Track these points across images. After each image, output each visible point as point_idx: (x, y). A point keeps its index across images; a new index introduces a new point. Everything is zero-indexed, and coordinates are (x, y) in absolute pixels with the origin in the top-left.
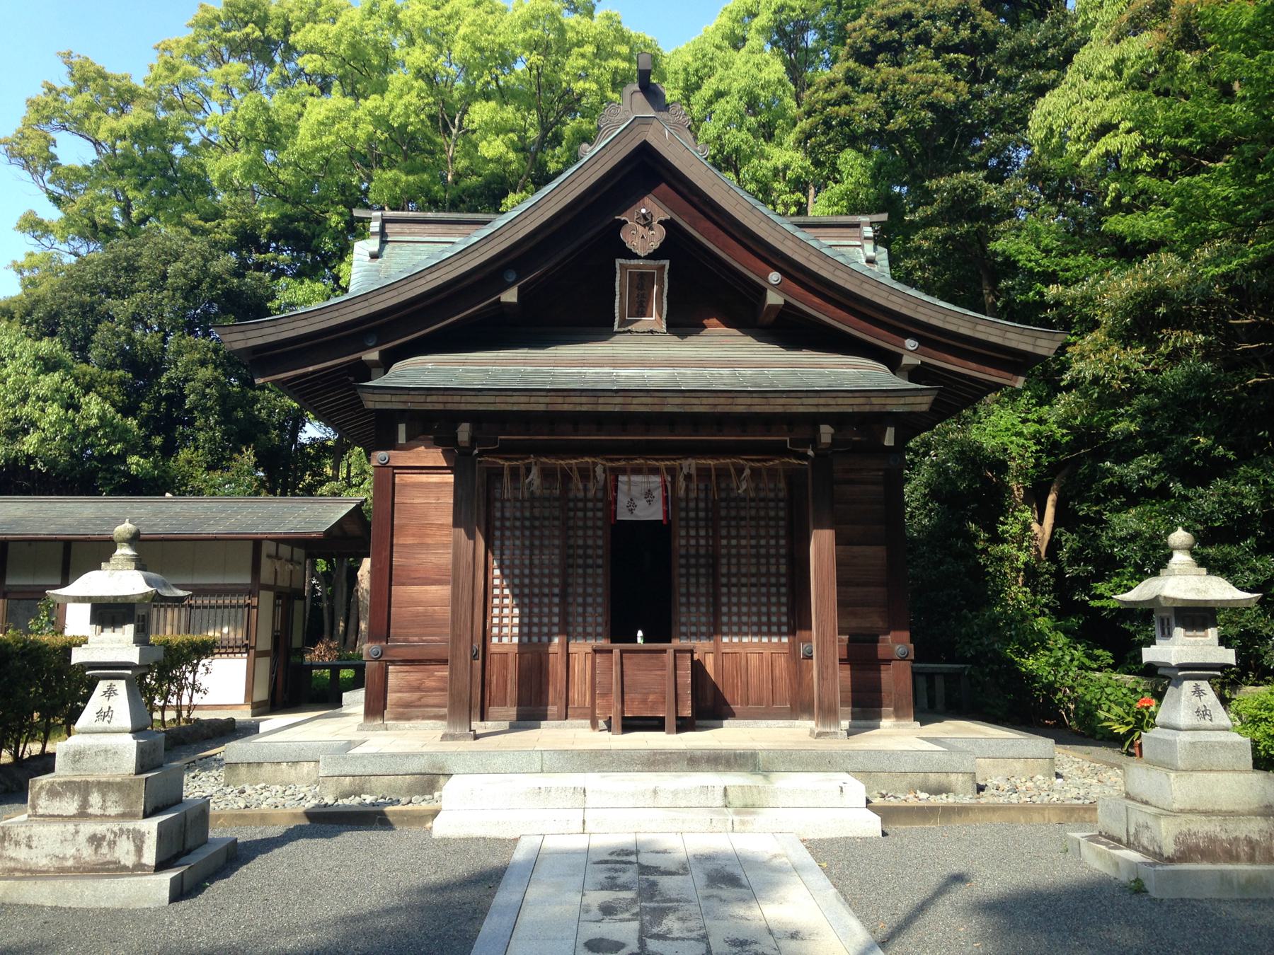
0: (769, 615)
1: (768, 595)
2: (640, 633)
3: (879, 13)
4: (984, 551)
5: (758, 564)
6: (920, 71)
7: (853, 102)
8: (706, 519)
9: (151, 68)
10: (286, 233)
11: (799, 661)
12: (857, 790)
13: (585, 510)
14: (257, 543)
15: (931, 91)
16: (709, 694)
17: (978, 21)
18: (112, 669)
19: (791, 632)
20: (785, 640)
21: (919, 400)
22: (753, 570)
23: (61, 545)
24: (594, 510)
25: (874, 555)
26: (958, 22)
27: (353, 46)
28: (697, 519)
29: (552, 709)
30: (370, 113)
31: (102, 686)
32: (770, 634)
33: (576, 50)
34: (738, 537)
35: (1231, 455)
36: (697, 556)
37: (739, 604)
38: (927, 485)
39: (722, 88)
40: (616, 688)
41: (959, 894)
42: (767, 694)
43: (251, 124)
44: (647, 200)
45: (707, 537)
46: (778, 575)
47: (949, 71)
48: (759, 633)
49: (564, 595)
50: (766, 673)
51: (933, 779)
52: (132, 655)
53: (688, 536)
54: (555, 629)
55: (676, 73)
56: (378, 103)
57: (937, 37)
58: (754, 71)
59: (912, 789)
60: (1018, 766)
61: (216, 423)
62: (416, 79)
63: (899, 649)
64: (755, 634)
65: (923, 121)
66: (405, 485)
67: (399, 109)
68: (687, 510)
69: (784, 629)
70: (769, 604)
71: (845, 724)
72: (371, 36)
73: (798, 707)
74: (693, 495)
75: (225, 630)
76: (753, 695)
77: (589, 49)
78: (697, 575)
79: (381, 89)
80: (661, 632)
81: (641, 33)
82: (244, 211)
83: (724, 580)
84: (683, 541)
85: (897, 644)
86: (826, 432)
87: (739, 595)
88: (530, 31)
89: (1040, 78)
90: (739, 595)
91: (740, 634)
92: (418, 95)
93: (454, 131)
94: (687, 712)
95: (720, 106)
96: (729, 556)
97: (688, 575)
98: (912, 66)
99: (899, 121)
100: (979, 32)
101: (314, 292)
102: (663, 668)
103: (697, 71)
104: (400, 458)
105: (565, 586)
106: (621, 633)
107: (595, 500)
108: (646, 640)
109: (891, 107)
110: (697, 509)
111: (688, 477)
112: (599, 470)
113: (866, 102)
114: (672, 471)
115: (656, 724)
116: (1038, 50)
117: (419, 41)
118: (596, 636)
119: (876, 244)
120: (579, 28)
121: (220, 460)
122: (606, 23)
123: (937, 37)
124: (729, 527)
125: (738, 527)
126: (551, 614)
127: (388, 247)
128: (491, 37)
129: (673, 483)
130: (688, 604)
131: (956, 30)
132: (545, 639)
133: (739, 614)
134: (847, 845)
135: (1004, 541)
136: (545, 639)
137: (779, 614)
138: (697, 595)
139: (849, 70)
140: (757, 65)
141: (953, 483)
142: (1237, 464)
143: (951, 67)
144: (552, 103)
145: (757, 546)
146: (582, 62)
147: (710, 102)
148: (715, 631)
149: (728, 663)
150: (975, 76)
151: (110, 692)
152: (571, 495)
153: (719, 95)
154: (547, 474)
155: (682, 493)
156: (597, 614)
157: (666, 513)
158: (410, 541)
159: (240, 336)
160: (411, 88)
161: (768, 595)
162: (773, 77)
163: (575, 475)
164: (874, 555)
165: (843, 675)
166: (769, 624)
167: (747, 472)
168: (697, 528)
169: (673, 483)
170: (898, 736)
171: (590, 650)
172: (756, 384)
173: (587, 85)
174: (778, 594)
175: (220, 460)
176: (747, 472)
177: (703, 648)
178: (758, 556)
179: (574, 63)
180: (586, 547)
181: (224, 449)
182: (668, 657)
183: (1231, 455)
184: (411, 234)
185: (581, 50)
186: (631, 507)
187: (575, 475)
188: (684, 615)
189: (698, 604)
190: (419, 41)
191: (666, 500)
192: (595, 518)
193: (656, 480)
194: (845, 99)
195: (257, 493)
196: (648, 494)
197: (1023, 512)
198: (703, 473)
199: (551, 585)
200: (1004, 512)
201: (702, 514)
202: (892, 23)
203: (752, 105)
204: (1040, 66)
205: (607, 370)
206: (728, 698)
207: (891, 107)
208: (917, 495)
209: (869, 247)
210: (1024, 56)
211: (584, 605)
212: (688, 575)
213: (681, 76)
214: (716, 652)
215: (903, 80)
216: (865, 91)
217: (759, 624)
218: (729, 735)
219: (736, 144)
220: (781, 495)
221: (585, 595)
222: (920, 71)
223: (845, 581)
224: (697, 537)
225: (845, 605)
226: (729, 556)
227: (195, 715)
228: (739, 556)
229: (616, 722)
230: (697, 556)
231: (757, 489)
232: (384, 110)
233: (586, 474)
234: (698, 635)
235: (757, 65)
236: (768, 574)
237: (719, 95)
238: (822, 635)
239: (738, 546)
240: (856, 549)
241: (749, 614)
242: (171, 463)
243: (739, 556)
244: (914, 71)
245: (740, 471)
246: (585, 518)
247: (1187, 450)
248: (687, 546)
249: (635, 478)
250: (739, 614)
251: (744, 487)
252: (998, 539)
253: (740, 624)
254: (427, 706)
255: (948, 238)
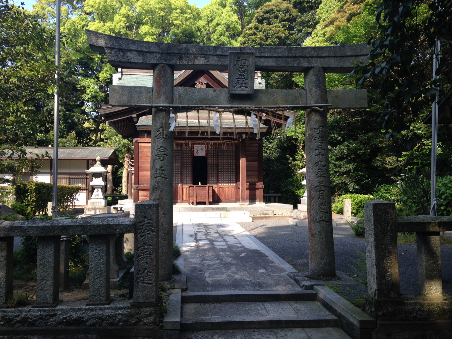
0: (230, 178)
1: (230, 174)
2: (200, 183)
3: (264, 8)
4: (291, 163)
5: (228, 166)
6: (275, 27)
7: (256, 35)
8: (216, 156)
9: (34, 7)
10: (81, 63)
11: (237, 189)
12: (248, 214)
13: (186, 153)
14: (88, 161)
15: (278, 33)
16: (216, 197)
17: (291, 13)
18: (98, 186)
19: (236, 183)
20: (234, 184)
21: (264, 129)
22: (227, 168)
23: (86, 161)
24: (188, 153)
25: (256, 164)
26: (286, 13)
27: (104, 6)
28: (213, 155)
29: (179, 201)
30: (109, 27)
31: (96, 190)
32: (231, 183)
33: (174, 11)
34: (223, 160)
35: (342, 140)
36: (213, 164)
37: (223, 176)
38: (277, 144)
39: (219, 23)
40: (195, 195)
41: (265, 226)
42: (230, 197)
43: (70, 30)
44: (202, 78)
45: (216, 160)
46: (233, 169)
47: (283, 27)
48: (228, 183)
49: (181, 174)
50: (230, 192)
51: (265, 212)
52: (103, 183)
53: (211, 160)
54: (179, 182)
55: (204, 16)
56: (111, 24)
57: (280, 17)
58: (228, 18)
59: (260, 214)
60: (285, 211)
61: (62, 123)
62: (123, 17)
63: (261, 186)
64: (227, 183)
65: (276, 42)
66: (142, 147)
67: (118, 27)
68: (211, 153)
69: (234, 182)
70: (230, 176)
71: (248, 203)
72: (110, 3)
73: (237, 200)
74: (212, 150)
75: (80, 185)
76: (226, 197)
77: (178, 11)
78: (213, 169)
79: (112, 20)
80: (205, 183)
81: (194, 6)
82: (68, 56)
83: (220, 170)
84: (210, 161)
85: (260, 185)
86: (244, 136)
87: (223, 174)
88: (161, 5)
89: (308, 30)
90: (223, 174)
91: (224, 183)
92: (124, 23)
93: (134, 31)
94: (211, 200)
95: (218, 28)
96: (221, 164)
97: (211, 169)
98: (273, 25)
99: (269, 41)
100: (291, 16)
101: (91, 82)
102: (206, 190)
103: (211, 17)
104: (140, 140)
105: (181, 171)
106: (195, 183)
107: (189, 151)
108: (201, 184)
109: (267, 37)
110: (213, 153)
111: (211, 145)
112: (190, 144)
113: (260, 35)
114: (207, 144)
115: (204, 203)
116: (308, 22)
117: (124, 5)
118: (189, 183)
119: (261, 78)
120: (175, 4)
121: (63, 135)
122: (184, 3)
123: (280, 17)
124: (221, 157)
125: (223, 157)
126: (178, 178)
127: (123, 76)
128: (148, 6)
129: (208, 147)
130: (211, 176)
131: (285, 15)
132: (177, 184)
133: (223, 178)
134: (245, 223)
135: (296, 160)
136: (177, 184)
137: (233, 178)
138: (213, 174)
139: (255, 25)
140: (229, 16)
141: (283, 144)
142: (343, 141)
143: (284, 26)
144: (165, 25)
145: (228, 162)
146: (176, 15)
147: (215, 27)
148: (218, 182)
149: (221, 190)
150: (290, 28)
151: (98, 191)
152: (183, 149)
153: (218, 25)
154: (177, 144)
155: (210, 149)
156: (189, 179)
157: (206, 154)
158: (143, 161)
159: (103, 111)
160: (121, 20)
161: (230, 174)
162: (234, 20)
163: (184, 145)
164: (256, 164)
165: (248, 192)
166: (231, 181)
167: (226, 144)
168: (213, 158)
169: (208, 147)
170: (260, 205)
171: (188, 187)
172: (227, 125)
173: (178, 22)
174: (233, 174)
175: (63, 135)
176: (226, 144)
177: (215, 187)
178: (228, 164)
179: (174, 14)
180: (186, 162)
181: (64, 131)
182: (207, 188)
183: (342, 140)
184: (130, 72)
185: (176, 11)
186: (197, 153)
187: (184, 145)
188: (210, 179)
189: (214, 176)
190: (124, 5)
191: (206, 151)
192: (188, 155)
193: (203, 146)
194: (254, 34)
195: (77, 146)
196: (202, 149)
197: (301, 152)
198: (215, 144)
199: (178, 171)
200: (297, 152)
201: (215, 154)
202: (267, 12)
203: (228, 28)
204: (309, 27)
205: (192, 120)
206: (221, 198)
207: (267, 37)
208: (274, 147)
209: (260, 79)
210: (304, 24)
211: (186, 176)
212: (211, 169)
213: (206, 18)
214: (218, 187)
215: (270, 29)
216: (260, 31)
217: (228, 181)
218: (221, 205)
219: (223, 41)
220: (234, 150)
221: (186, 174)
222: (275, 27)
223: (248, 170)
224: (213, 160)
225: (248, 176)
226: (221, 164)
227: (75, 207)
228: (223, 164)
229: (195, 203)
230: (213, 164)
231: (228, 148)
232: (113, 27)
233: (186, 144)
234: (213, 183)
235: (229, 16)
236: (230, 169)
237: (218, 25)
238: (242, 183)
239: (223, 162)
240: (251, 163)
241: (226, 178)
242: (48, 135)
243: (223, 164)
244: (274, 27)
245: (224, 144)
246: (186, 155)
247: (332, 138)
248: (211, 162)
249: (199, 145)
250: (223, 178)
251: (225, 148)
252: (295, 160)
253: (224, 181)
254: (253, 147)
255: (282, 75)
